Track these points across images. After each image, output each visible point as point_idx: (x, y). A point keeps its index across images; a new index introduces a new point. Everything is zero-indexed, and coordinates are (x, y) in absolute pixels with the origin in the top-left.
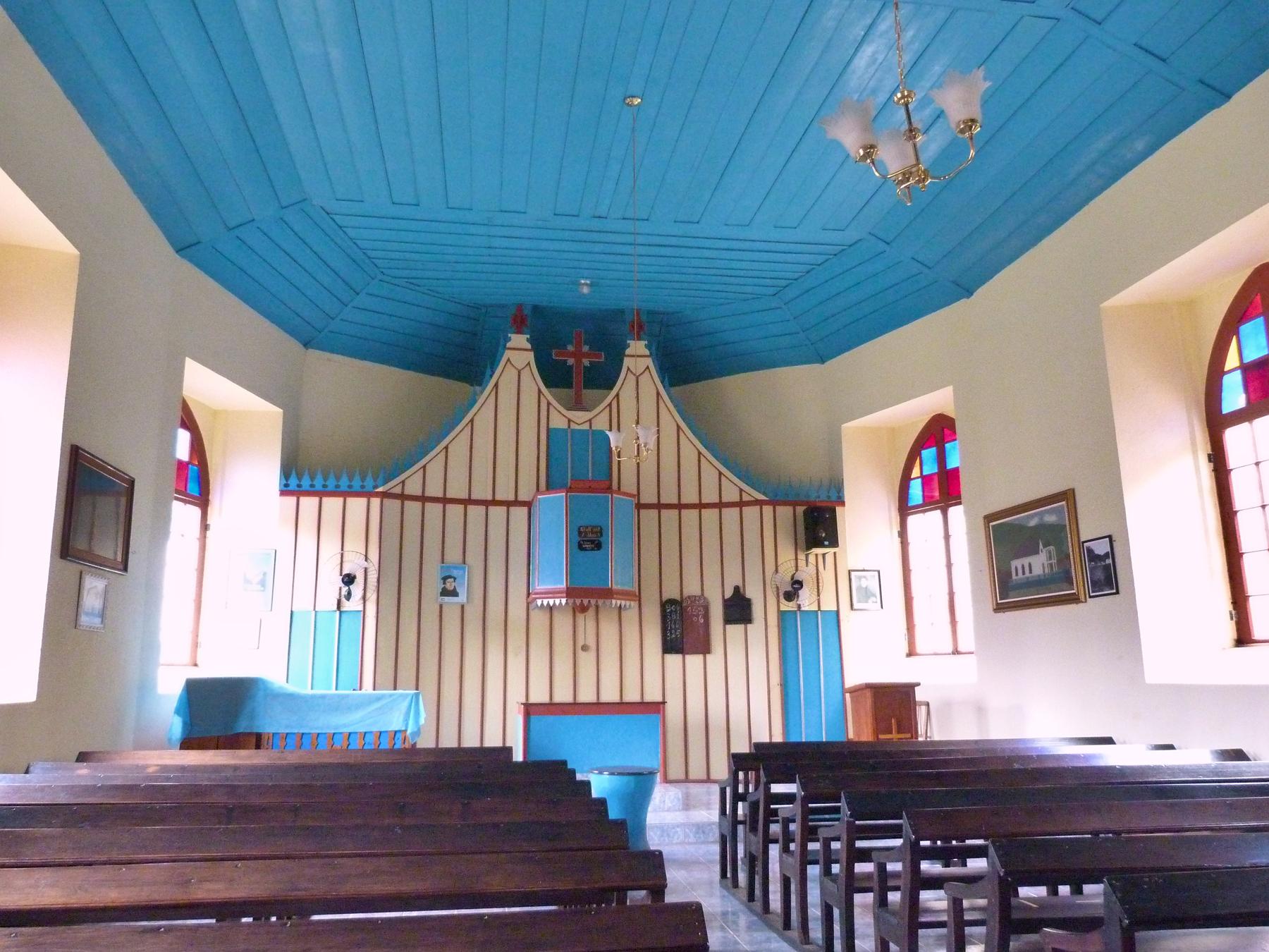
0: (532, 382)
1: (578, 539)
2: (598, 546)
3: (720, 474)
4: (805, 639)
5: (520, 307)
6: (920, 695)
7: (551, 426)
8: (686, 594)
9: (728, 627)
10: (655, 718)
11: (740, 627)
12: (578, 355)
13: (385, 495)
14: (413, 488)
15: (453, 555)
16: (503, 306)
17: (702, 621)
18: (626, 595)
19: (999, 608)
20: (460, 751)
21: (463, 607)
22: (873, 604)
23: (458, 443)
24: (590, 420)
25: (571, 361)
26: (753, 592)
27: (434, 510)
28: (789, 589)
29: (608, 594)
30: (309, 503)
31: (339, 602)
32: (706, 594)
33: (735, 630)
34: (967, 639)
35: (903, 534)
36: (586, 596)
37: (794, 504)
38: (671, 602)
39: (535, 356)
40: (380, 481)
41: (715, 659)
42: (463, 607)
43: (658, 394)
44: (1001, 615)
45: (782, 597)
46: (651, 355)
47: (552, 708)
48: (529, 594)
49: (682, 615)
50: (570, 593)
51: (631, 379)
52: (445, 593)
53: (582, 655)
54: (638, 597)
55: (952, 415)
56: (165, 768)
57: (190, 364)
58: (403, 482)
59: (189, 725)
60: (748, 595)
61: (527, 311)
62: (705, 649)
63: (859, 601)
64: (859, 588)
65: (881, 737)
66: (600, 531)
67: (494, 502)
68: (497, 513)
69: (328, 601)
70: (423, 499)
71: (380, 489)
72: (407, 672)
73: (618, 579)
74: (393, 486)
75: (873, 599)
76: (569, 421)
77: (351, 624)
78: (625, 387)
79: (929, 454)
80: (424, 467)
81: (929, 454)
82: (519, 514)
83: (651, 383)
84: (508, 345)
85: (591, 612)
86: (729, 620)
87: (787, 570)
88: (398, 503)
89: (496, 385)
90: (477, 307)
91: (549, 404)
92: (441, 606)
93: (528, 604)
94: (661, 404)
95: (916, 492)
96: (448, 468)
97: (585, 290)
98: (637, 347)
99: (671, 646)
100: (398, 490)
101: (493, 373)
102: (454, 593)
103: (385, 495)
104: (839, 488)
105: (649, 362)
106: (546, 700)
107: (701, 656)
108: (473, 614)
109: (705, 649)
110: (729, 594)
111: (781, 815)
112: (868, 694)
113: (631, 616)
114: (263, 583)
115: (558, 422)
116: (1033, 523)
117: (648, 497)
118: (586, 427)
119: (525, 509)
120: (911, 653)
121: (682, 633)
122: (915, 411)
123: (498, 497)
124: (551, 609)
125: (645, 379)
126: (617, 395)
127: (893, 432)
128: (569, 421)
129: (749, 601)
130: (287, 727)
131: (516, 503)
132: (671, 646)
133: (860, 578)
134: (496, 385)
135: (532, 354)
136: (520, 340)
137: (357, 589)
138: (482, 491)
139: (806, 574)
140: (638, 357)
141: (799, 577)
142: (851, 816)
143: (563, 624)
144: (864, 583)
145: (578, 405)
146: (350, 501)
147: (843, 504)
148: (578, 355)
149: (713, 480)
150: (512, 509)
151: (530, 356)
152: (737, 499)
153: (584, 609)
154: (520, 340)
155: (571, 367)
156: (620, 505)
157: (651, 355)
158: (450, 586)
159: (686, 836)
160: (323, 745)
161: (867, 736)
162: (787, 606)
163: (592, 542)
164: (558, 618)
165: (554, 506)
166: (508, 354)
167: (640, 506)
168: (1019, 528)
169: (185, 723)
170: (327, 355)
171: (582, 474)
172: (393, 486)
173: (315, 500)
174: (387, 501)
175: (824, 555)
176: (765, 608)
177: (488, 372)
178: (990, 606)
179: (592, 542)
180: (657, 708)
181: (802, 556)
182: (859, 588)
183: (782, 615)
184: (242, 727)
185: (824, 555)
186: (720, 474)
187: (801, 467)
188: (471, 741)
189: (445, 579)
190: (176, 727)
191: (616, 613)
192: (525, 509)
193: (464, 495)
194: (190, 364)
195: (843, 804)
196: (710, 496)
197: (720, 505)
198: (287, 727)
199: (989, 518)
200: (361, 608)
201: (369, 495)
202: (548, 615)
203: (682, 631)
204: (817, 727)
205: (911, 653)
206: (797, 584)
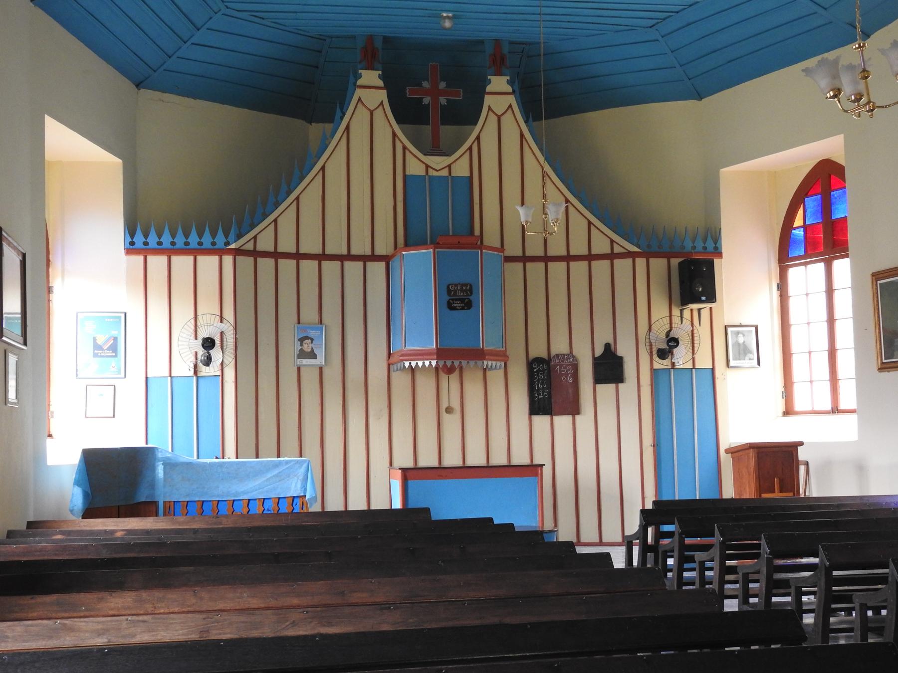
0: (386, 125)
1: (446, 298)
2: (468, 305)
3: (590, 223)
4: (681, 395)
5: (370, 38)
6: (803, 454)
9: (598, 386)
10: (532, 480)
11: (611, 387)
12: (435, 92)
13: (238, 252)
14: (265, 243)
15: (309, 313)
16: (353, 37)
17: (571, 380)
19: (884, 367)
20: (346, 513)
21: (321, 369)
22: (749, 362)
23: (309, 192)
24: (449, 166)
26: (625, 350)
27: (286, 266)
28: (664, 346)
29: (479, 354)
30: (157, 262)
31: (196, 366)
32: (575, 352)
34: (848, 397)
35: (783, 287)
36: (456, 356)
37: (668, 256)
38: (539, 360)
40: (232, 236)
41: (584, 420)
42: (321, 369)
43: (522, 135)
44: (885, 374)
45: (655, 356)
46: (514, 92)
47: (440, 472)
48: (389, 355)
50: (441, 353)
51: (493, 119)
52: (302, 354)
53: (445, 417)
54: (502, 356)
55: (841, 161)
56: (129, 532)
57: (48, 119)
58: (255, 238)
59: (88, 497)
60: (620, 353)
61: (378, 44)
62: (574, 409)
63: (735, 359)
64: (737, 344)
65: (765, 496)
66: (469, 289)
68: (353, 269)
69: (183, 367)
70: (276, 255)
71: (233, 246)
73: (488, 340)
74: (245, 243)
75: (751, 356)
76: (427, 167)
77: (210, 391)
79: (812, 202)
80: (275, 221)
81: (812, 202)
82: (377, 269)
83: (514, 125)
84: (359, 82)
85: (457, 373)
86: (600, 378)
87: (660, 328)
88: (250, 260)
89: (347, 128)
90: (321, 38)
91: (404, 148)
92: (299, 369)
93: (389, 365)
96: (298, 221)
97: (447, 24)
98: (499, 83)
99: (540, 406)
100: (250, 246)
101: (344, 114)
102: (312, 355)
103: (238, 252)
104: (717, 239)
105: (512, 100)
106: (435, 464)
107: (570, 418)
109: (574, 409)
110: (599, 352)
111: (696, 559)
112: (752, 453)
113: (496, 378)
115: (415, 168)
118: (445, 173)
119: (382, 265)
120: (787, 413)
121: (550, 394)
122: (802, 157)
123: (354, 252)
124: (413, 370)
125: (508, 119)
126: (478, 138)
127: (774, 176)
128: (427, 167)
129: (621, 358)
130: (188, 495)
131: (374, 257)
132: (540, 406)
133: (738, 333)
134: (347, 128)
136: (371, 77)
137: (216, 354)
138: (337, 246)
139: (681, 331)
141: (673, 334)
142: (770, 554)
143: (426, 386)
144: (741, 339)
145: (435, 149)
146: (201, 259)
147: (720, 255)
148: (434, 91)
149: (585, 233)
150: (369, 264)
151: (383, 95)
152: (608, 251)
153: (450, 371)
154: (371, 77)
155: (420, 85)
156: (489, 260)
157: (514, 92)
158: (307, 347)
160: (224, 510)
161: (749, 493)
162: (659, 364)
163: (462, 301)
164: (420, 379)
165: (419, 264)
166: (359, 93)
169: (86, 495)
170: (158, 94)
171: (443, 224)
172: (245, 243)
173: (164, 259)
174: (239, 259)
175: (699, 310)
176: (638, 366)
177: (338, 113)
178: (874, 364)
179: (462, 301)
180: (533, 469)
181: (676, 312)
182: (737, 344)
183: (655, 373)
184: (142, 497)
185: (699, 310)
186: (590, 223)
187: (679, 216)
188: (357, 503)
189: (302, 340)
190: (76, 497)
191: (480, 374)
192: (382, 265)
193: (318, 250)
194: (48, 119)
195: (763, 542)
196: (579, 247)
197: (590, 258)
198: (188, 495)
199: (877, 276)
200: (219, 373)
201: (222, 253)
202: (410, 376)
203: (550, 390)
204: (689, 487)
205: (787, 413)
206: (673, 342)
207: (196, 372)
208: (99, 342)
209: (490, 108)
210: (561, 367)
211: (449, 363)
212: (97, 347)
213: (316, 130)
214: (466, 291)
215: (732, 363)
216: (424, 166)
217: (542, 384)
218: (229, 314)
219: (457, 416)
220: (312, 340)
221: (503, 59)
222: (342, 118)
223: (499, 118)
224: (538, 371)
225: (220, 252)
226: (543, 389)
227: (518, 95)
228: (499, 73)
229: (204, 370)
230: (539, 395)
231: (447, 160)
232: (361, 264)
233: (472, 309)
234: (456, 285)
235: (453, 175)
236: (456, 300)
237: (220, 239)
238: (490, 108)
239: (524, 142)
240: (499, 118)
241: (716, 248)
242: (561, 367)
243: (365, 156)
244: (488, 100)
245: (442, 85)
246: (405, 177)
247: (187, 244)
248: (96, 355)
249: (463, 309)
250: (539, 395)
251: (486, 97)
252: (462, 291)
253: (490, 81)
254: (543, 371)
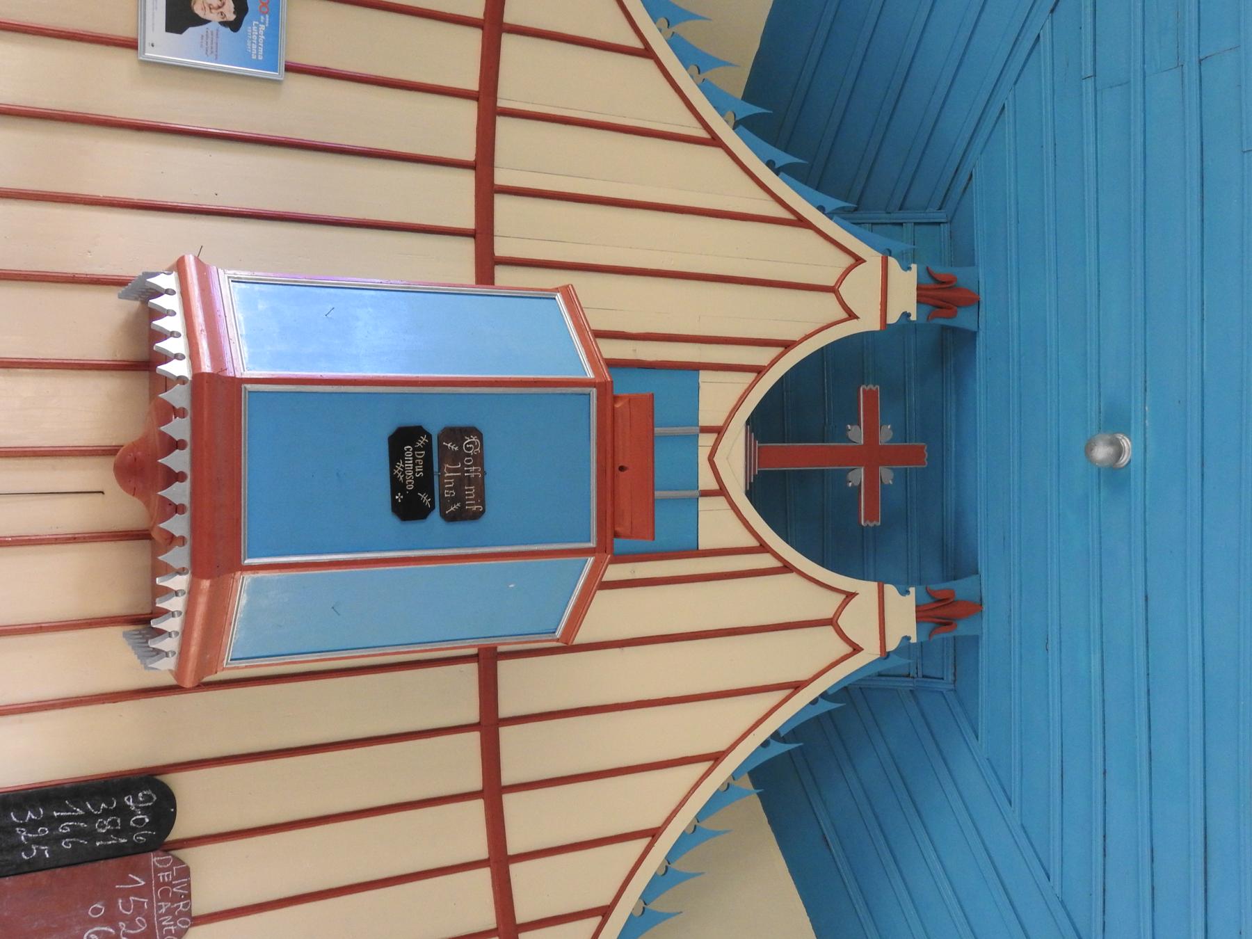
0: (807, 324)
2: (409, 506)
5: (973, 301)
7: (704, 376)
18: (212, 623)
21: (131, 44)
24: (722, 491)
25: (857, 434)
38: (164, 808)
39: (873, 333)
43: (797, 686)
49: (118, 852)
50: (218, 393)
51: (825, 605)
54: (198, 677)
66: (464, 511)
67: (487, 192)
76: (719, 431)
78: (803, 590)
85: (123, 509)
89: (801, 222)
91: (760, 371)
97: (1102, 452)
101: (830, 216)
105: (870, 653)
108: (109, 84)
113: (112, 660)
117: (521, 686)
118: (706, 481)
126: (787, 568)
128: (719, 431)
134: (801, 222)
135: (875, 326)
140: (882, 617)
151: (869, 322)
153: (138, 468)
157: (886, 655)
163: (425, 483)
167: (487, 661)
177: (833, 203)
179: (425, 483)
209: (850, 596)
210: (138, 892)
211: (178, 461)
214: (460, 498)
216: (719, 422)
217: (76, 833)
220: (235, 26)
221: (946, 623)
222: (821, 209)
223: (832, 622)
224: (124, 812)
226: (54, 840)
227: (880, 668)
228: (922, 614)
230: (32, 826)
231: (736, 484)
232: (469, 223)
233: (393, 521)
234: (479, 460)
235: (702, 501)
236: (428, 462)
238: (850, 596)
239: (787, 692)
240: (832, 622)
242: (138, 892)
244: (866, 589)
245: (858, 476)
246: (696, 367)
249: (394, 481)
250: (32, 826)
251: (872, 586)
252: (461, 482)
253: (905, 592)
254: (126, 830)
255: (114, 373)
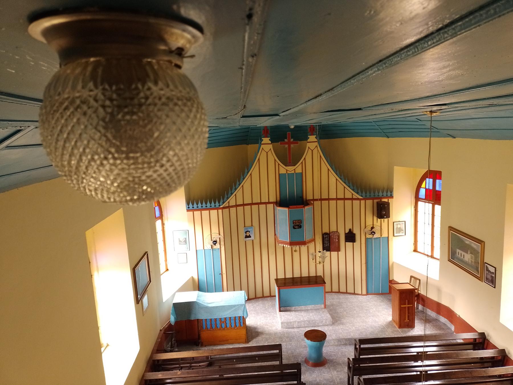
0: (272, 157)
2: (300, 227)
8: (331, 231)
13: (224, 208)
15: (248, 223)
23: (246, 183)
26: (356, 231)
29: (304, 243)
30: (197, 213)
33: (349, 244)
40: (221, 203)
41: (342, 253)
51: (310, 151)
52: (247, 237)
53: (294, 253)
60: (354, 232)
62: (338, 250)
64: (397, 228)
66: (300, 221)
67: (261, 203)
68: (262, 207)
69: (208, 246)
71: (221, 207)
72: (213, 135)
74: (226, 204)
77: (217, 253)
84: (262, 143)
87: (369, 223)
91: (279, 164)
94: (322, 161)
95: (422, 193)
96: (244, 193)
100: (227, 205)
102: (250, 237)
103: (224, 208)
105: (316, 144)
108: (257, 242)
109: (338, 250)
110: (347, 231)
114: (185, 241)
115: (283, 171)
116: (467, 242)
118: (293, 172)
125: (315, 152)
126: (305, 159)
129: (355, 234)
133: (398, 224)
138: (256, 200)
144: (399, 226)
155: (284, 141)
158: (248, 235)
159: (334, 343)
163: (298, 226)
166: (262, 146)
168: (462, 241)
172: (226, 204)
179: (298, 226)
182: (397, 228)
189: (246, 232)
197: (344, 199)
203: (329, 243)
205: (415, 250)
207: (212, 248)
208: (181, 240)
212: (180, 241)
213: (251, 148)
215: (395, 235)
218: (222, 233)
219: (298, 253)
225: (217, 209)
229: (215, 247)
231: (294, 167)
237: (217, 204)
241: (391, 195)
243: (266, 171)
245: (292, 140)
247: (206, 207)
248: (180, 244)
255: (378, 296)
